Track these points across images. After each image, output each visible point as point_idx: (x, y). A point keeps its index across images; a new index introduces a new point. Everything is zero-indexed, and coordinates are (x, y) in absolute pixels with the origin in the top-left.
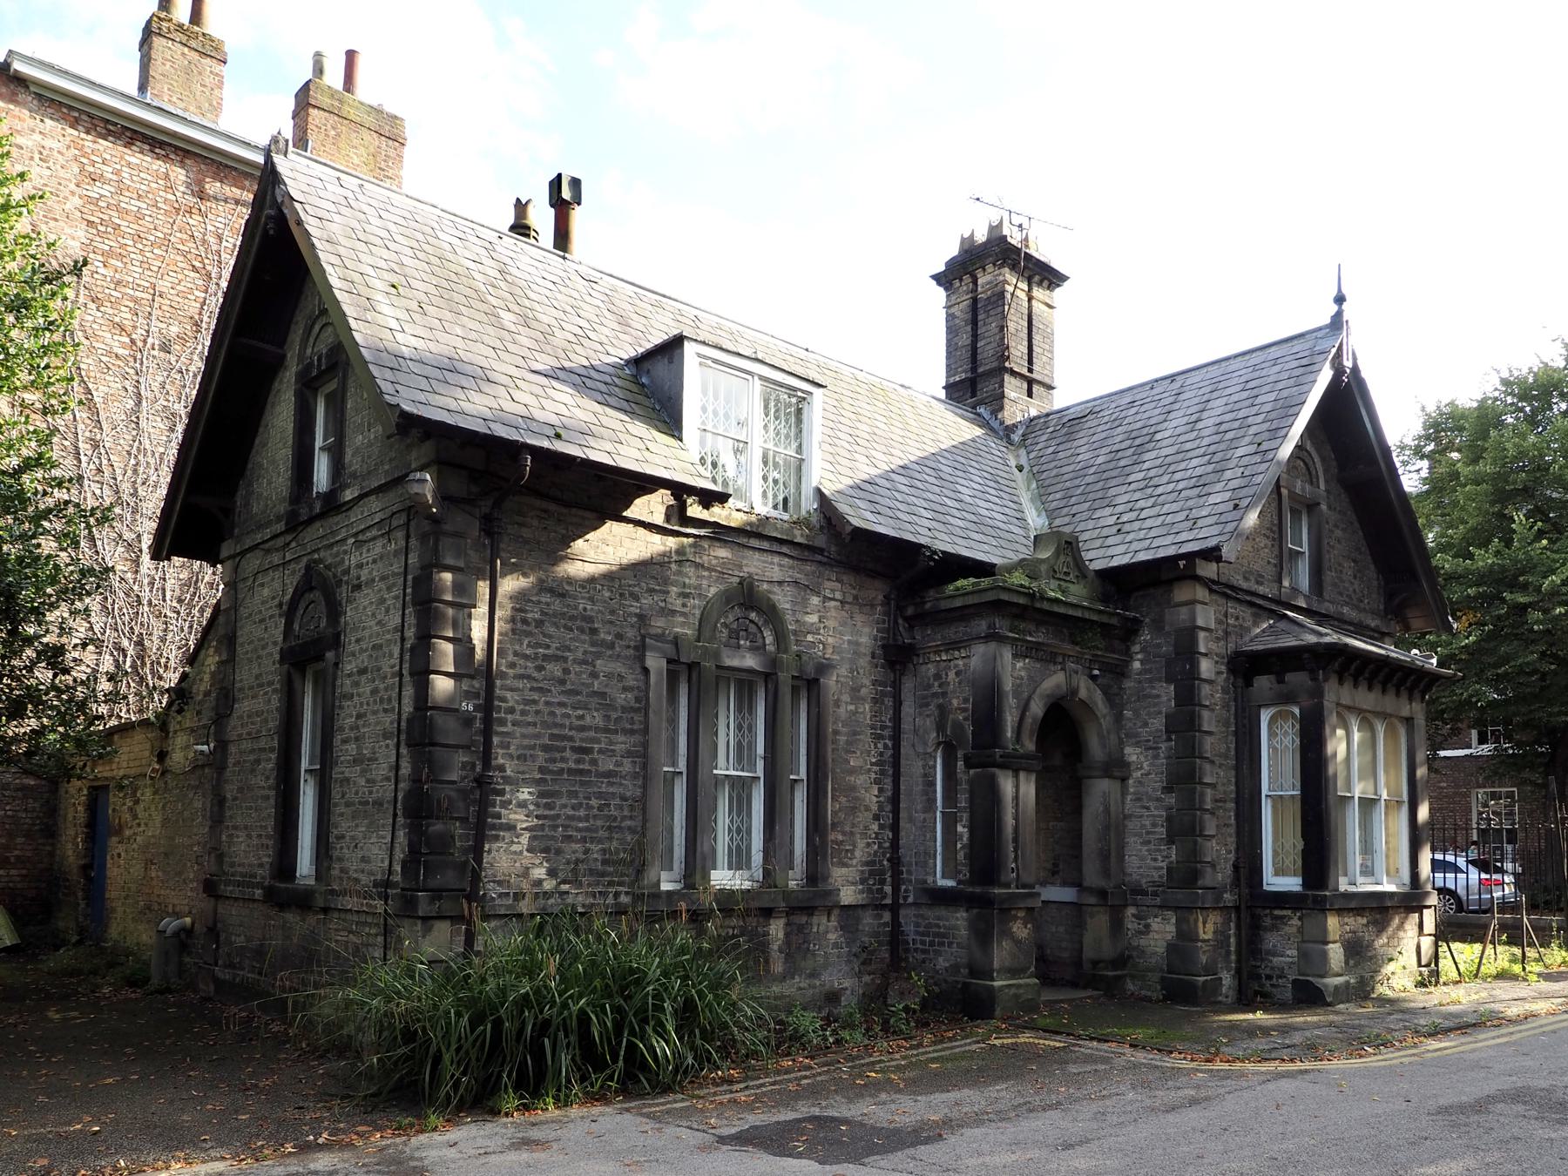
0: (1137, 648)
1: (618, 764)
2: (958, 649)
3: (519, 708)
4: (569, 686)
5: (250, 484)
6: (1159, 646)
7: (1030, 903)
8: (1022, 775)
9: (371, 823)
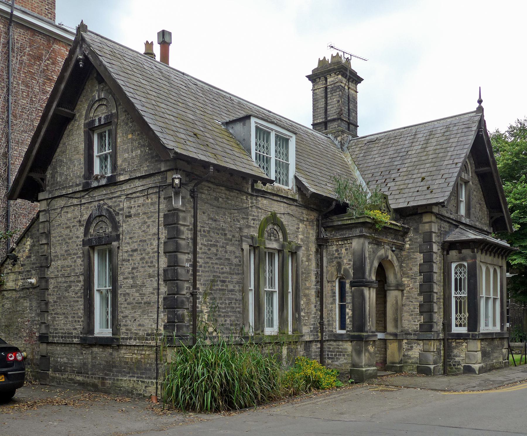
0: (407, 239)
1: (234, 287)
2: (347, 240)
3: (203, 265)
4: (218, 256)
5: (55, 168)
6: (417, 239)
7: (374, 339)
8: (371, 289)
9: (144, 311)
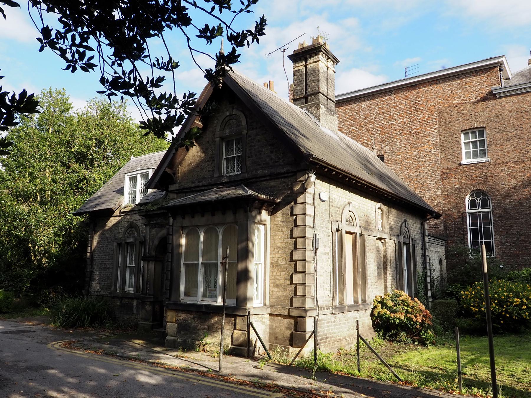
8: (150, 262)
